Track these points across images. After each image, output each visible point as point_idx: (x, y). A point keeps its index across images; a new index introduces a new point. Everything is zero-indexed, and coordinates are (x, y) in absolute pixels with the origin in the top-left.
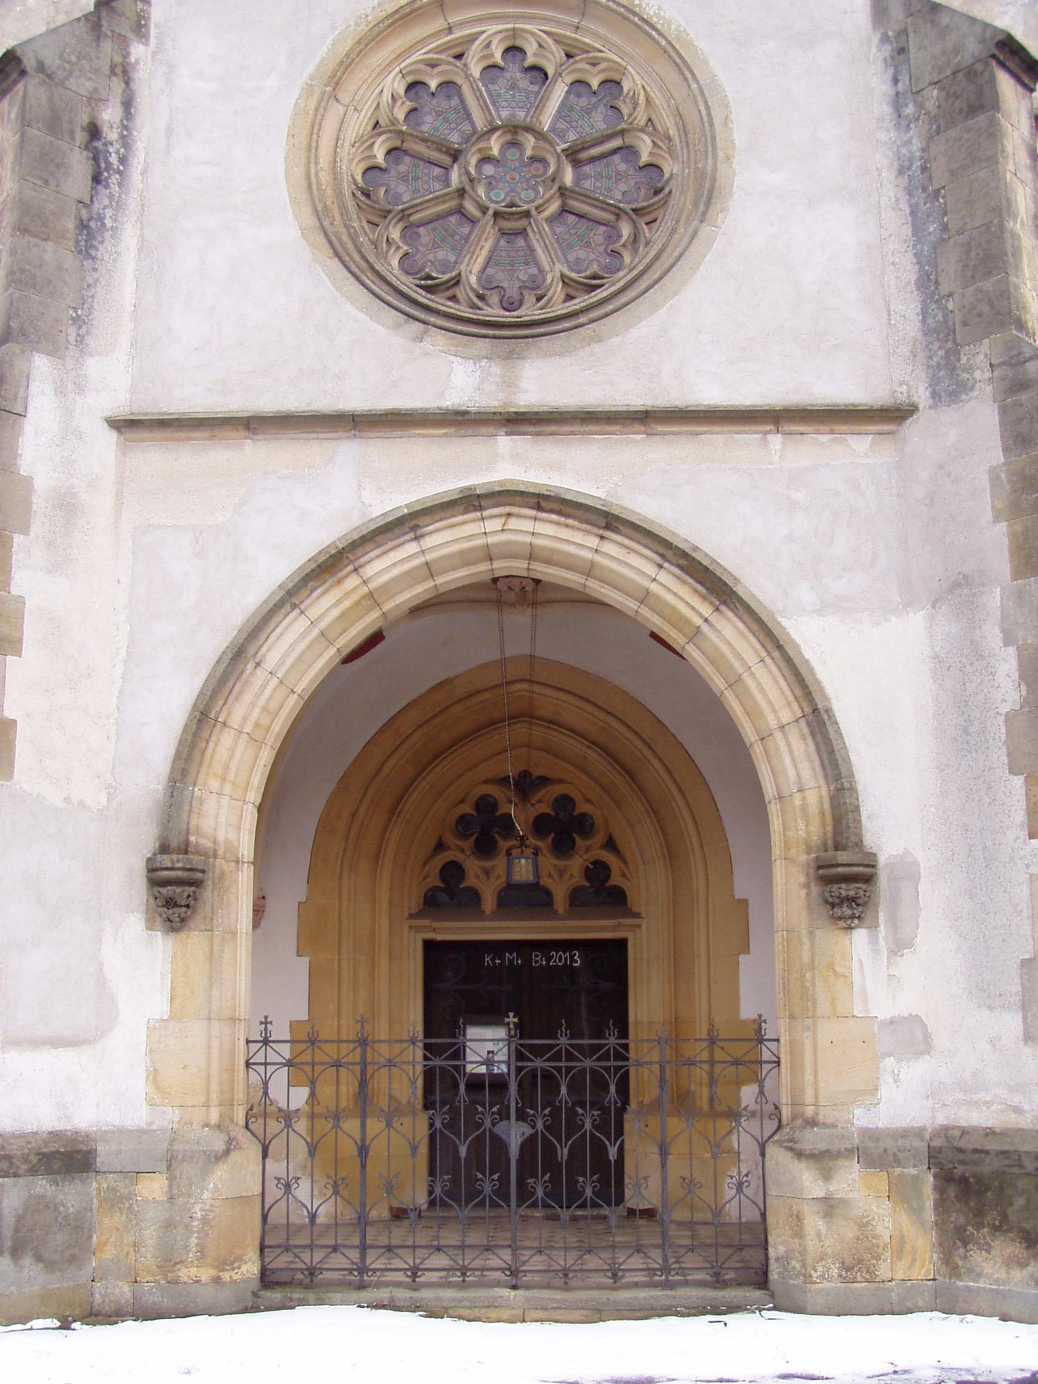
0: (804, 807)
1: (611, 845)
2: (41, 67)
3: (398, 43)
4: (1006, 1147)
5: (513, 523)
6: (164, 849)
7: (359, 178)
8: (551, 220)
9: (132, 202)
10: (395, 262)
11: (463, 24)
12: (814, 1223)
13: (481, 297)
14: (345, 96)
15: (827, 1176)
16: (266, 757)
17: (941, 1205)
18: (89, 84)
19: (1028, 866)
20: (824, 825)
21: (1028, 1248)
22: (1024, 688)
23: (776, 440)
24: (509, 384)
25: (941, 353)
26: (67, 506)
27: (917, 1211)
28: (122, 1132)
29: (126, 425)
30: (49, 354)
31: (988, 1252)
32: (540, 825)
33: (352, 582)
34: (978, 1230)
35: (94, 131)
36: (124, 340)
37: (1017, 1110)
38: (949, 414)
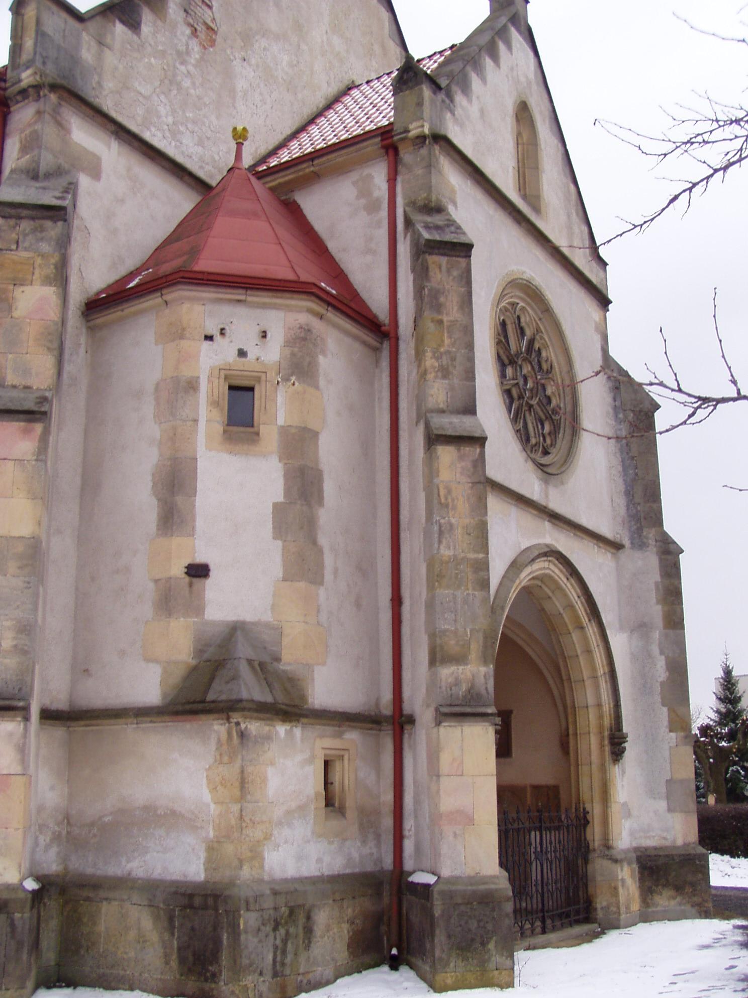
4: (667, 853)
19: (669, 743)
20: (611, 720)
21: (676, 891)
22: (667, 674)
25: (635, 527)
31: (661, 895)
34: (657, 887)
37: (665, 838)
38: (638, 554)
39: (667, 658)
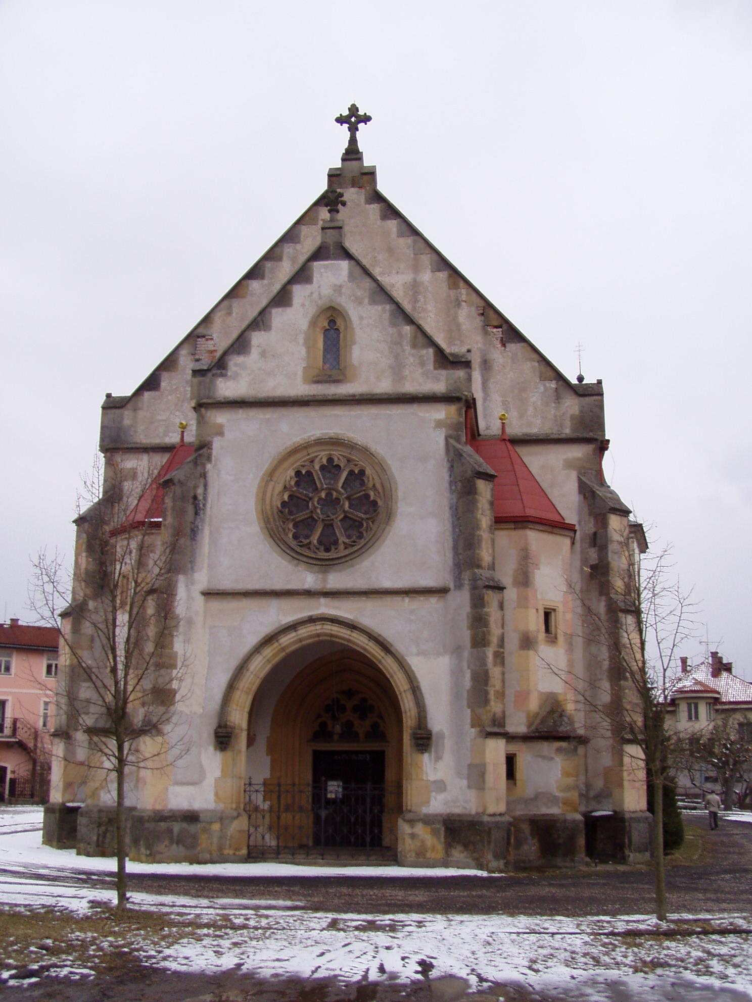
0: (410, 716)
1: (380, 716)
2: (179, 481)
3: (291, 460)
5: (325, 627)
6: (219, 726)
7: (279, 506)
8: (341, 520)
9: (207, 519)
10: (291, 535)
11: (313, 453)
12: (408, 841)
13: (318, 549)
14: (274, 479)
15: (412, 827)
16: (250, 698)
17: (446, 837)
18: (193, 483)
23: (407, 600)
24: (325, 581)
26: (190, 622)
27: (438, 838)
28: (207, 811)
29: (208, 594)
30: (183, 574)
32: (355, 709)
33: (276, 645)
35: (195, 498)
36: (206, 565)
37: (465, 808)
39: (472, 670)
